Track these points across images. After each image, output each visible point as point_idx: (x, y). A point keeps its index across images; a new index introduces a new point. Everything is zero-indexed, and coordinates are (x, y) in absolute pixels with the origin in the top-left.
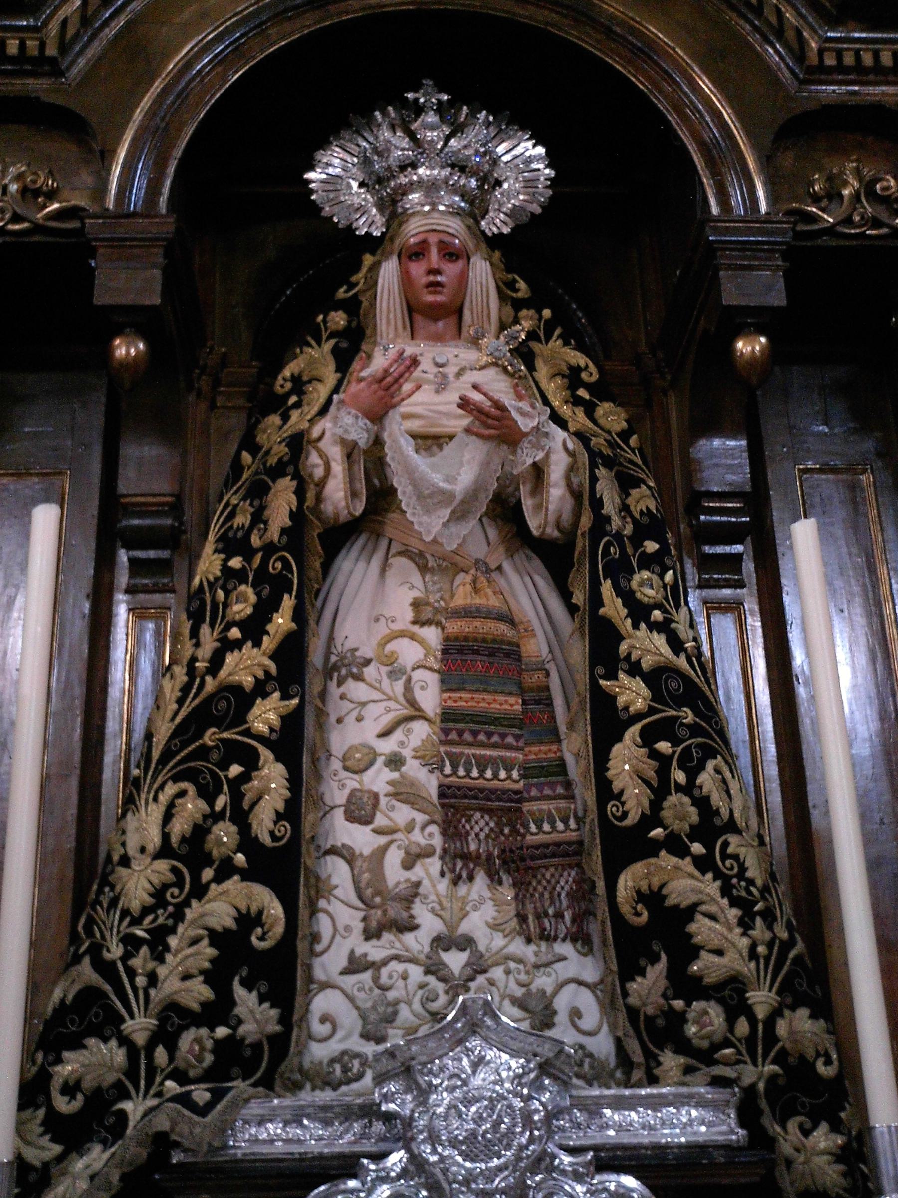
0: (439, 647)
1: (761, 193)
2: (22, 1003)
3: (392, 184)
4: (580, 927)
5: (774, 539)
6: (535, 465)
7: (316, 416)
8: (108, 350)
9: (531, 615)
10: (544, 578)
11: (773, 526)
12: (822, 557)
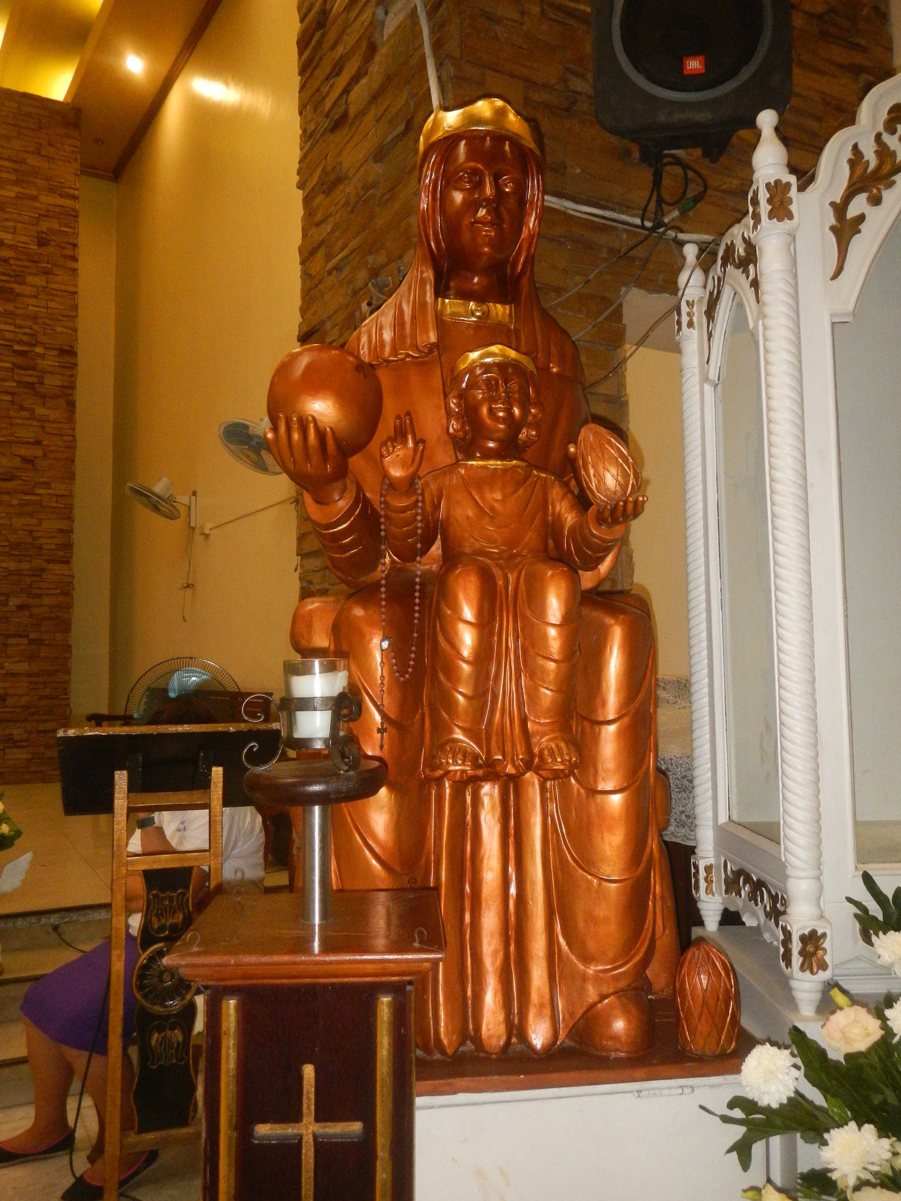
0: (224, 879)
4: (55, 397)
6: (376, 161)
8: (682, 66)
9: (801, 853)
10: (381, 1043)
11: (480, 1075)
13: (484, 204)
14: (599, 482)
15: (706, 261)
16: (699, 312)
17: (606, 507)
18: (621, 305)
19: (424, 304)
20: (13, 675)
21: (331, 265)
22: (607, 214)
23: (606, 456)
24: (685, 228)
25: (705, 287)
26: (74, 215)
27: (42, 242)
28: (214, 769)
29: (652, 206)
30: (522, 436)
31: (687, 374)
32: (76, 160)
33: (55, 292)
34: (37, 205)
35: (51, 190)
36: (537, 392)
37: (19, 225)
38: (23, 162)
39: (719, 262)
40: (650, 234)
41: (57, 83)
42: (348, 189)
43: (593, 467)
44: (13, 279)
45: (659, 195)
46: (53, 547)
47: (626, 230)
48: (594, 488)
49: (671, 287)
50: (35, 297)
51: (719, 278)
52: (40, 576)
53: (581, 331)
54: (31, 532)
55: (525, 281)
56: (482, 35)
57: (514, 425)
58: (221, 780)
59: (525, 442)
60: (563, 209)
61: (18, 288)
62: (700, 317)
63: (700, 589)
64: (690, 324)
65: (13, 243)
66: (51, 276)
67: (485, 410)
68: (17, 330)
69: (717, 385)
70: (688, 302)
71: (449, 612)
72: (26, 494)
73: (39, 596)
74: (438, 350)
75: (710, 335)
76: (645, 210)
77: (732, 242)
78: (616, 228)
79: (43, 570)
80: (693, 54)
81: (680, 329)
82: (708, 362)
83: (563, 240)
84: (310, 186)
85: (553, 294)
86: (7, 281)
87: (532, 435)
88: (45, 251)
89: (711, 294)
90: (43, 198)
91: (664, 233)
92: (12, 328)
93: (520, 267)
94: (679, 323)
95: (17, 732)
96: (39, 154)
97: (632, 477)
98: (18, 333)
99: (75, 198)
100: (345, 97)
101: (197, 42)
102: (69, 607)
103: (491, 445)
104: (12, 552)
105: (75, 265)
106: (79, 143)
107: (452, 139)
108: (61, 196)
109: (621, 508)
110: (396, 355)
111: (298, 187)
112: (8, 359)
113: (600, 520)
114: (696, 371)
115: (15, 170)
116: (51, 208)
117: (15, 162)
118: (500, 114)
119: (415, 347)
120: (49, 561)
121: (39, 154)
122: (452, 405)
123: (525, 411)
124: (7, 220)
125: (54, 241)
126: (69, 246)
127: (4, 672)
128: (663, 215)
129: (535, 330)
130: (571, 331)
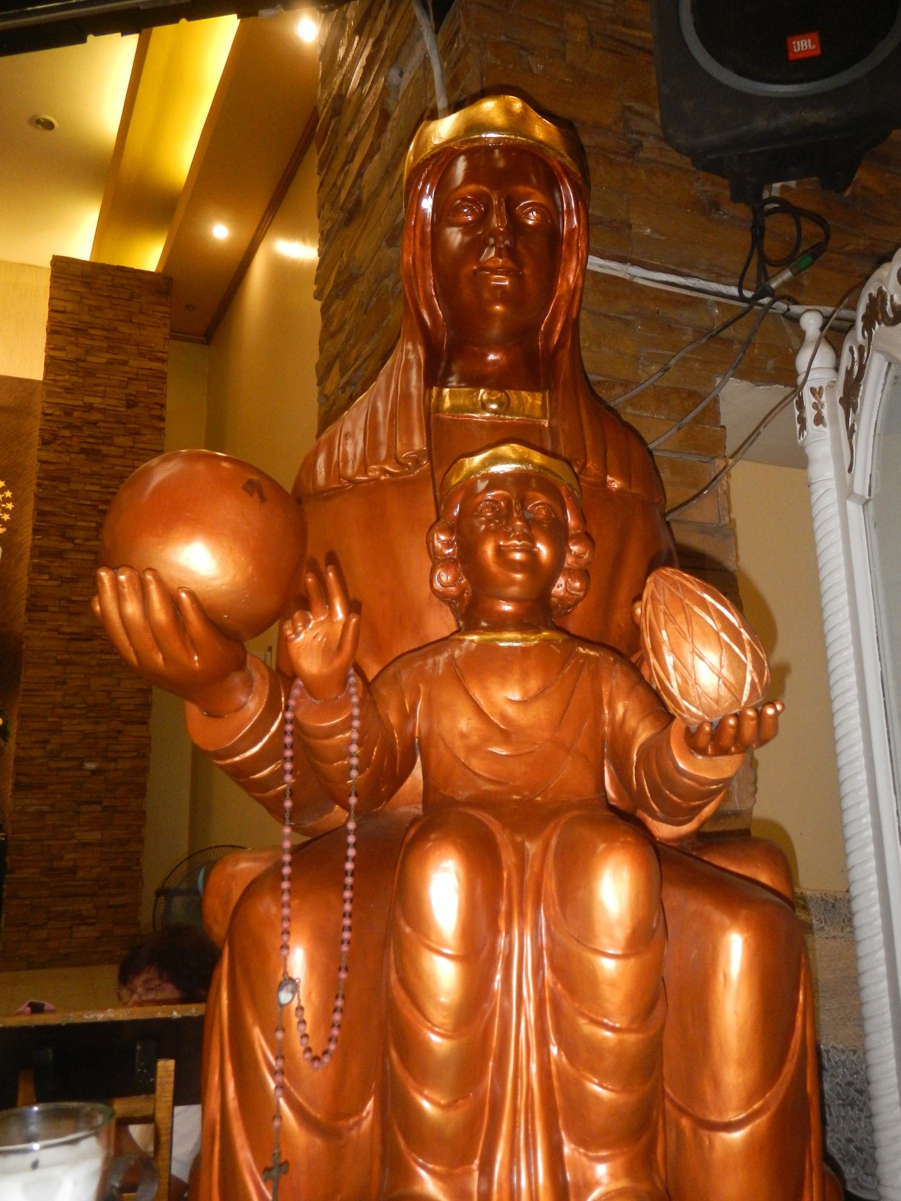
1: (675, 798)
2: (146, 60)
3: (103, 728)
5: (188, 177)
7: (738, 606)
8: (785, 49)
12: (872, 1131)
13: (492, 241)
14: (685, 680)
15: (835, 334)
16: (831, 405)
17: (700, 728)
18: (716, 401)
19: (406, 396)
20: (85, 845)
21: (345, 378)
22: (690, 282)
23: (696, 629)
24: (799, 299)
25: (837, 369)
26: (162, 377)
27: (130, 405)
28: (161, 1063)
29: (753, 271)
30: (560, 587)
31: (818, 491)
32: (165, 325)
33: (141, 452)
34: (127, 369)
35: (142, 355)
36: (582, 517)
37: (109, 389)
38: (115, 329)
39: (860, 324)
40: (750, 308)
41: (149, 256)
42: (361, 288)
43: (672, 651)
44: (101, 441)
45: (762, 254)
46: (131, 707)
47: (718, 303)
48: (675, 691)
49: (787, 375)
50: (122, 457)
51: (861, 349)
52: (116, 738)
53: (661, 435)
54: (109, 692)
55: (564, 356)
56: (511, 66)
57: (541, 576)
58: (172, 1079)
59: (561, 599)
60: (627, 277)
61: (105, 449)
62: (832, 406)
63: (862, 806)
64: (819, 420)
65: (103, 406)
66: (137, 437)
67: (489, 550)
68: (105, 490)
69: (867, 502)
70: (813, 390)
71: (408, 930)
72: (106, 654)
73: (115, 760)
74: (430, 460)
75: (851, 432)
76: (742, 277)
77: (880, 291)
78: (705, 300)
79: (119, 732)
80: (801, 31)
81: (803, 427)
82: (850, 470)
83: (630, 318)
84: (326, 293)
85: (619, 390)
86: (94, 443)
87: (575, 589)
88: (136, 411)
89: (849, 372)
90: (131, 362)
91: (770, 305)
92: (98, 488)
93: (556, 338)
94: (802, 420)
95: (86, 907)
96: (131, 322)
97: (750, 667)
98: (103, 493)
99: (164, 361)
100: (359, 182)
101: (279, 206)
102: (146, 770)
103: (507, 608)
104: (90, 715)
105: (161, 425)
106: (168, 310)
107: (445, 156)
108: (150, 360)
109: (731, 731)
110: (365, 473)
111: (316, 298)
112: (93, 519)
113: (692, 741)
114: (832, 484)
115: (106, 337)
116: (140, 372)
117: (108, 330)
118: (517, 124)
119: (393, 457)
120: (126, 723)
121: (131, 322)
122: (439, 545)
123: (559, 552)
124: (98, 385)
125: (142, 402)
126: (157, 407)
127: (76, 841)
128: (768, 279)
129: (581, 426)
130: (647, 437)
